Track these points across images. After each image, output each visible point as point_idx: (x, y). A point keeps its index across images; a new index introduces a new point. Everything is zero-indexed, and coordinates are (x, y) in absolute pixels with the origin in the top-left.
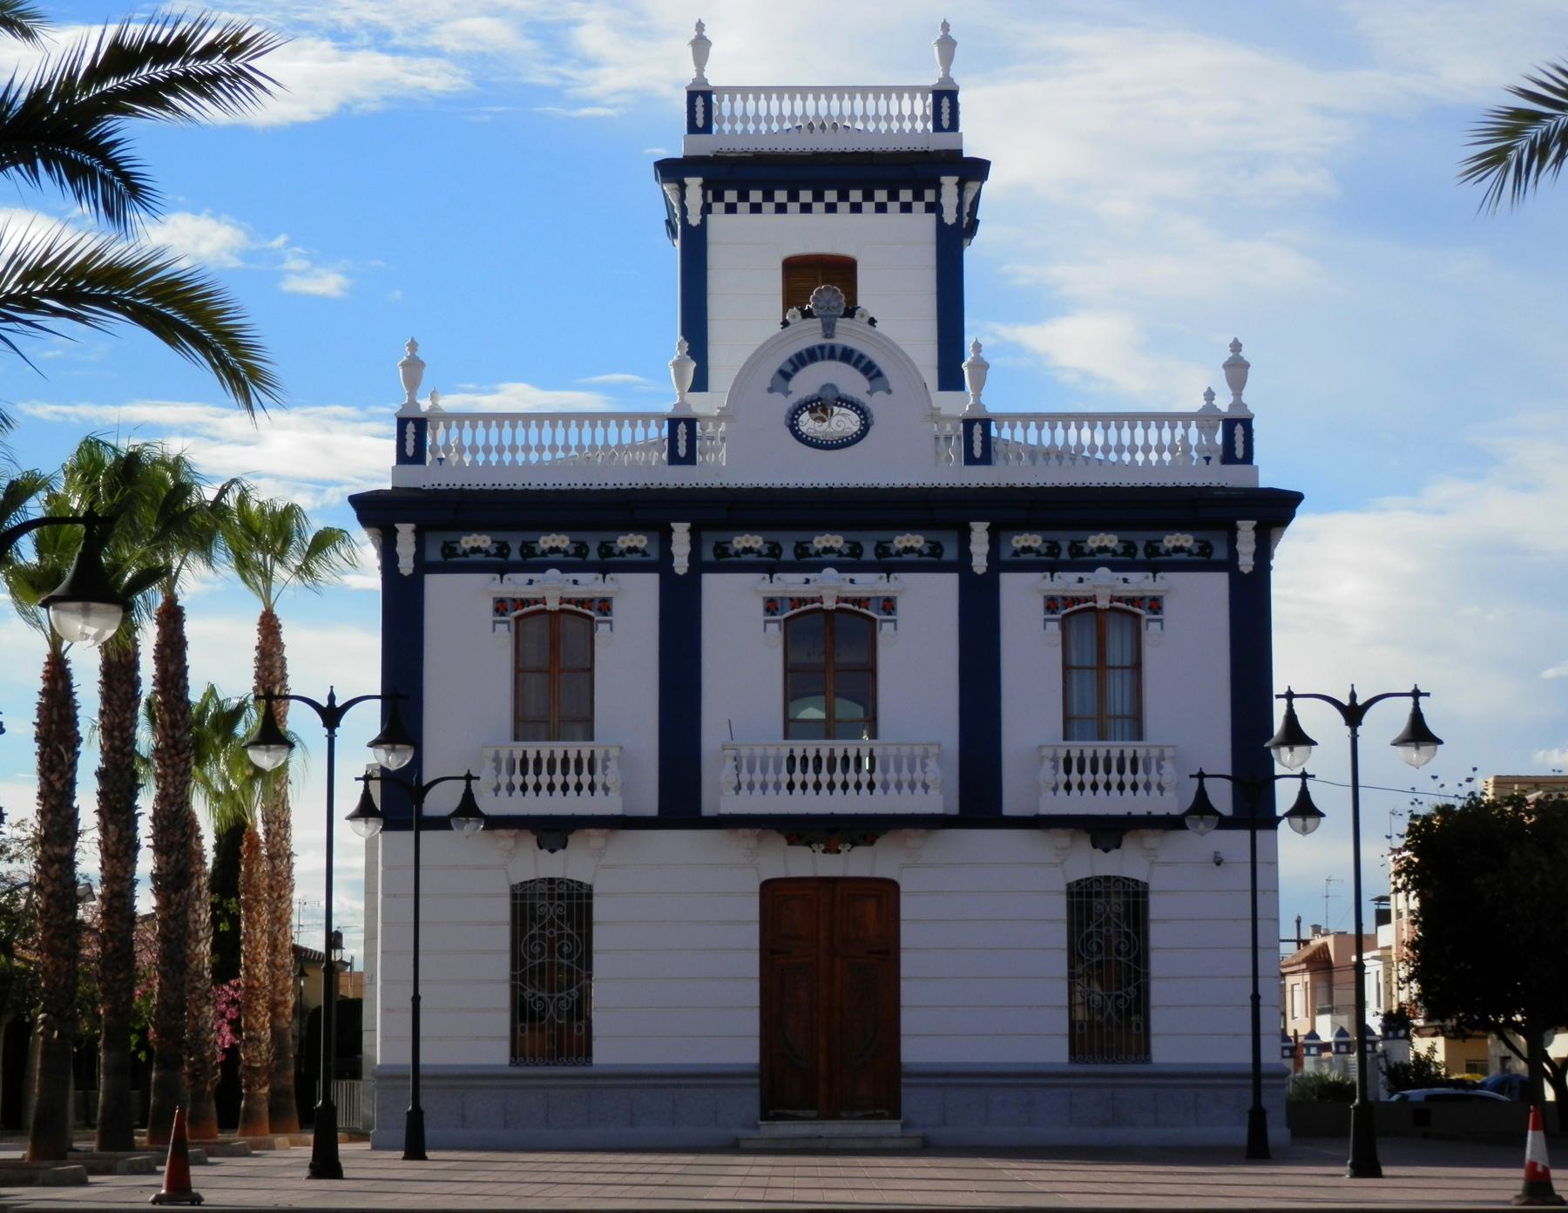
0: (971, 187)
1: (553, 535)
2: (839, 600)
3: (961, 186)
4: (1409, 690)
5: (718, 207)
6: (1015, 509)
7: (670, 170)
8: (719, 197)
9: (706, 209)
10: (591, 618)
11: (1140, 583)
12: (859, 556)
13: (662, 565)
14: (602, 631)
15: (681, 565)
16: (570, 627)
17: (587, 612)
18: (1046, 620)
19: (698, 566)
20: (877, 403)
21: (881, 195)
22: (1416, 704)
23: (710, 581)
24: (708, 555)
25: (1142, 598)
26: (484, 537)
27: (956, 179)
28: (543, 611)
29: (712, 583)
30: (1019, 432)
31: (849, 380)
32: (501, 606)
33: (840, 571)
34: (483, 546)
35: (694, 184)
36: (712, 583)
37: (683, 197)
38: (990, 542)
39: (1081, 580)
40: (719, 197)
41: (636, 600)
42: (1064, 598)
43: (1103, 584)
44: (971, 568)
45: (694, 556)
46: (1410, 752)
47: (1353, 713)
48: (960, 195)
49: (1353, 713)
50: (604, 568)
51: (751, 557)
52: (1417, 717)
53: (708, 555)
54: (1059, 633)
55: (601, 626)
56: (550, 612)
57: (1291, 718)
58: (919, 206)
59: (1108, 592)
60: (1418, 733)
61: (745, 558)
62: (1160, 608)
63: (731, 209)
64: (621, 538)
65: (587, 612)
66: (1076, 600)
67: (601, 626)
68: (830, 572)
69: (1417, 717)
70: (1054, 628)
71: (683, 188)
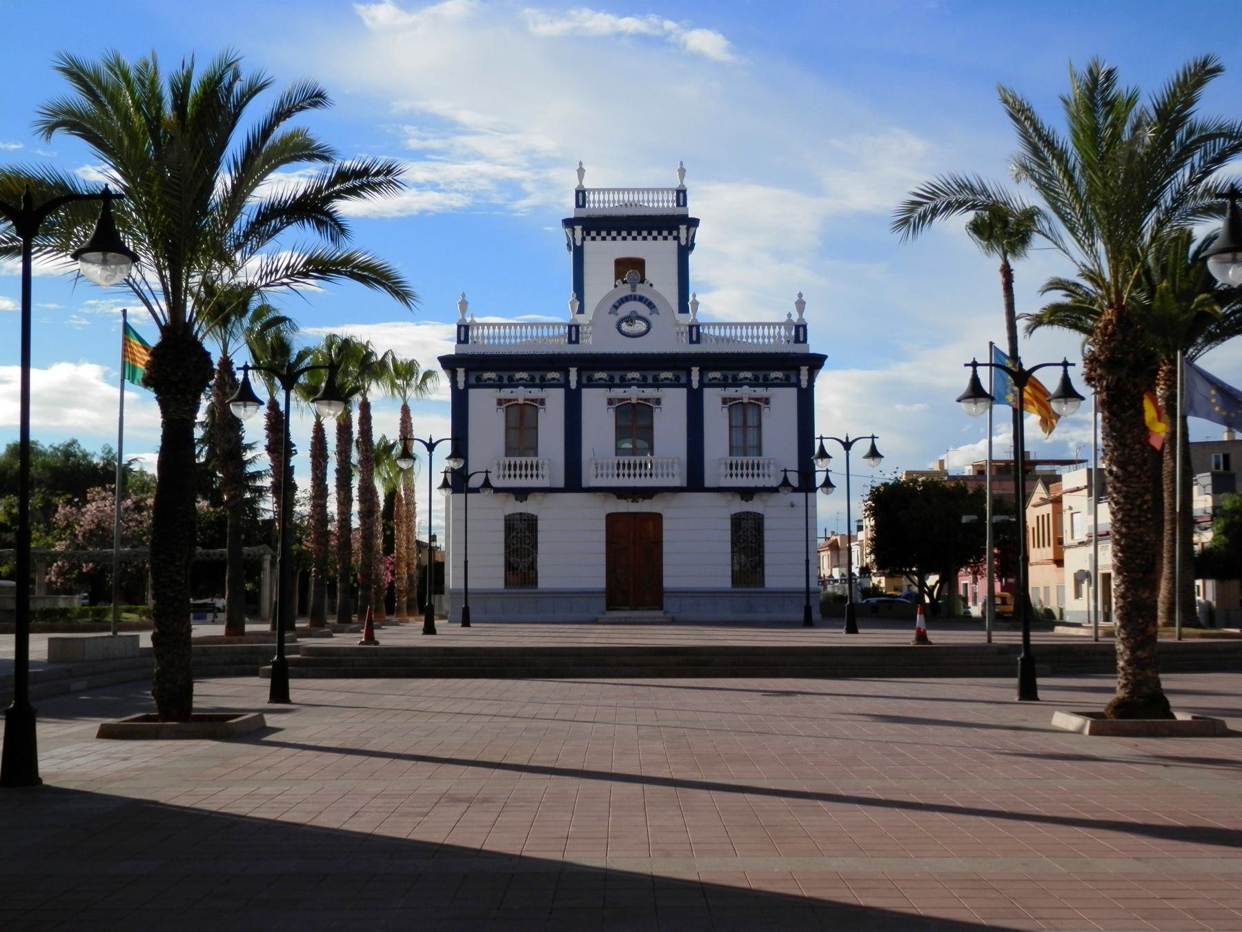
0: (692, 230)
3: (688, 229)
4: (1060, 361)
5: (588, 238)
6: (710, 362)
7: (568, 223)
8: (588, 234)
9: (583, 239)
11: (761, 392)
13: (566, 385)
14: (541, 412)
19: (580, 385)
20: (653, 318)
21: (634, 233)
22: (1065, 371)
23: (585, 391)
24: (584, 381)
29: (586, 393)
31: (642, 309)
32: (500, 402)
35: (578, 229)
36: (586, 393)
40: (588, 234)
41: (555, 399)
43: (746, 393)
45: (579, 381)
46: (870, 461)
47: (847, 445)
49: (847, 445)
52: (873, 447)
53: (584, 381)
57: (822, 447)
58: (670, 238)
60: (874, 453)
63: (593, 239)
66: (509, 400)
69: (873, 447)
70: (726, 410)
71: (574, 230)
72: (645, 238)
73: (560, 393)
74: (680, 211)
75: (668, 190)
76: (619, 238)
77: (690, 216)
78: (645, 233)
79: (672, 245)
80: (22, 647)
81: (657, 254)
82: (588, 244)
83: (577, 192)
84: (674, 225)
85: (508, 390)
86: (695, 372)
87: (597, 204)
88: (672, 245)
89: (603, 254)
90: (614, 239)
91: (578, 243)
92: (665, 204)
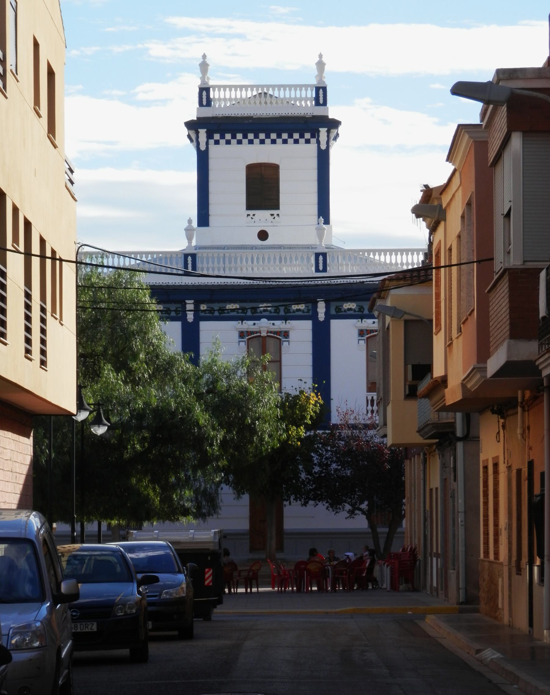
0: (333, 132)
1: (349, 303)
2: (268, 332)
3: (328, 132)
5: (211, 142)
6: (202, 294)
7: (190, 125)
8: (212, 138)
9: (207, 144)
10: (280, 339)
11: (279, 325)
12: (363, 312)
13: (313, 316)
14: (285, 344)
15: (321, 317)
16: (271, 343)
17: (278, 337)
18: (359, 340)
19: (329, 316)
21: (251, 136)
23: (203, 325)
24: (333, 312)
25: (281, 332)
26: (353, 304)
27: (326, 129)
28: (260, 336)
29: (335, 324)
30: (382, 257)
32: (242, 335)
33: (268, 320)
34: (301, 308)
35: (203, 133)
36: (335, 324)
37: (197, 137)
38: (326, 307)
39: (254, 324)
40: (212, 138)
41: (301, 332)
42: (367, 330)
43: (264, 326)
44: (318, 318)
45: (327, 313)
48: (328, 136)
50: (286, 318)
51: (351, 312)
53: (333, 312)
54: (365, 345)
55: (284, 343)
56: (263, 337)
58: (245, 141)
59: (266, 329)
61: (348, 312)
62: (288, 336)
64: (345, 304)
65: (278, 337)
66: (253, 333)
67: (284, 343)
68: (264, 320)
70: (363, 343)
71: (197, 133)
72: (296, 142)
73: (308, 325)
74: (319, 111)
75: (306, 86)
76: (302, 141)
77: (331, 116)
78: (228, 136)
79: (311, 149)
80: (251, 590)
81: (293, 159)
82: (213, 148)
83: (201, 90)
84: (312, 126)
85: (251, 323)
86: (190, 305)
87: (224, 103)
88: (311, 149)
89: (234, 159)
90: (285, 142)
91: (203, 148)
92: (305, 106)
